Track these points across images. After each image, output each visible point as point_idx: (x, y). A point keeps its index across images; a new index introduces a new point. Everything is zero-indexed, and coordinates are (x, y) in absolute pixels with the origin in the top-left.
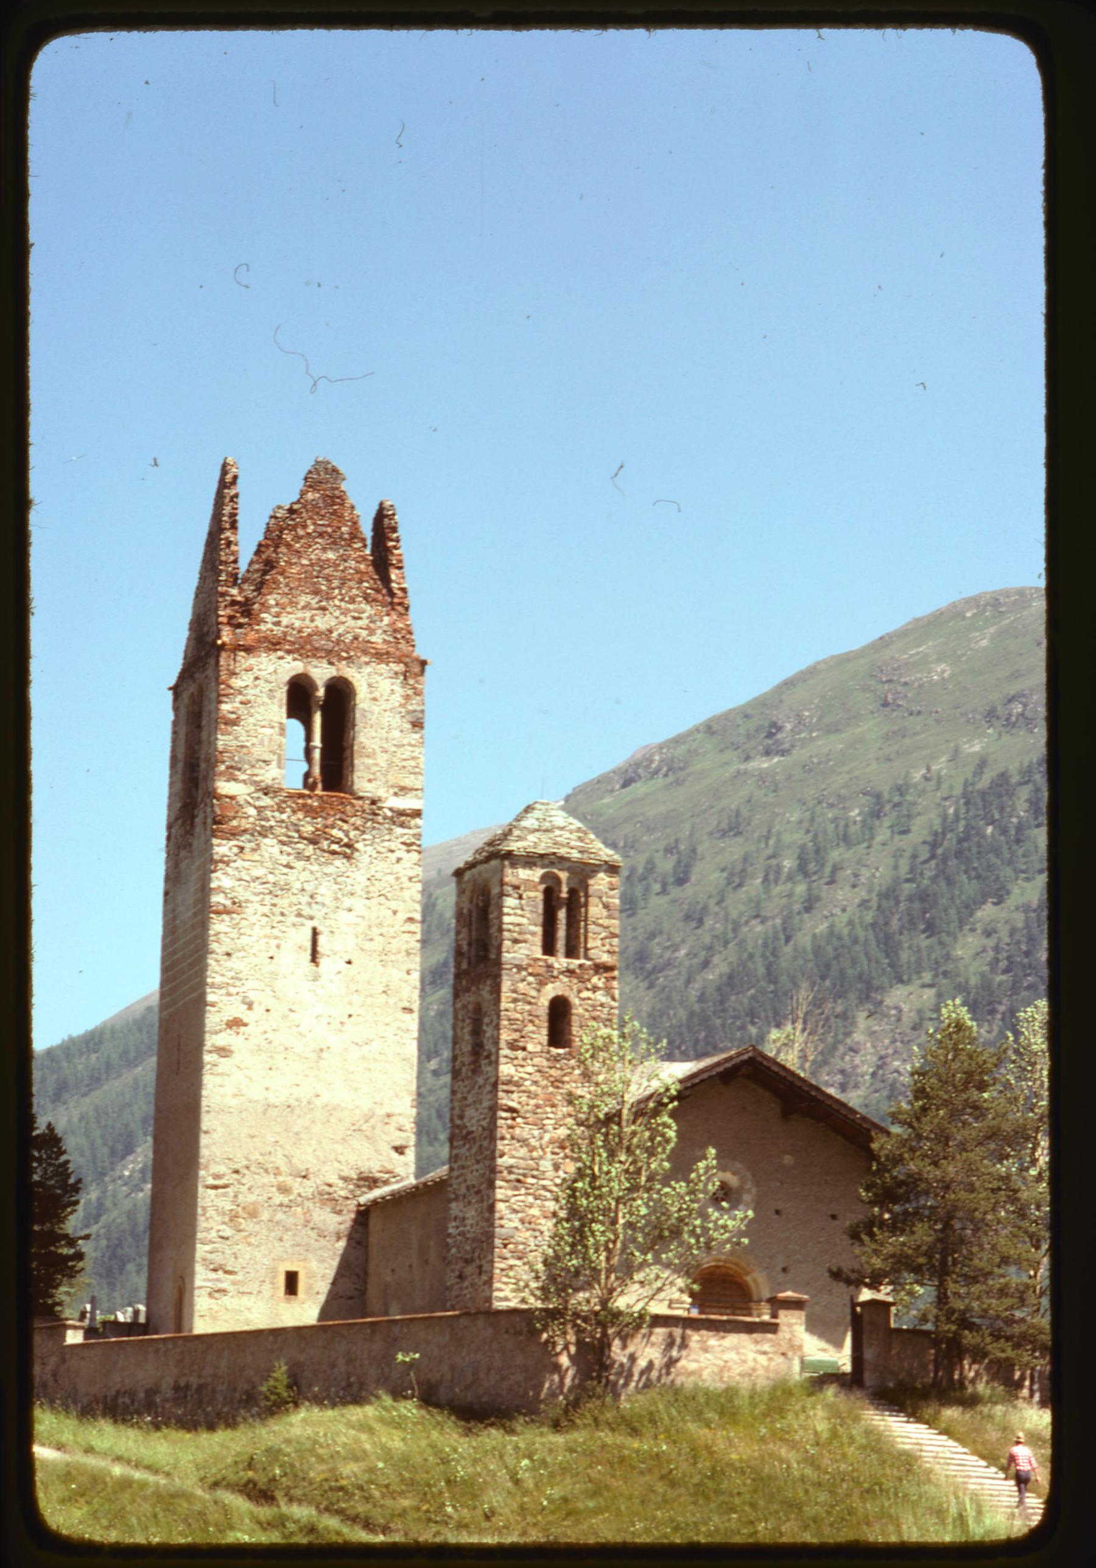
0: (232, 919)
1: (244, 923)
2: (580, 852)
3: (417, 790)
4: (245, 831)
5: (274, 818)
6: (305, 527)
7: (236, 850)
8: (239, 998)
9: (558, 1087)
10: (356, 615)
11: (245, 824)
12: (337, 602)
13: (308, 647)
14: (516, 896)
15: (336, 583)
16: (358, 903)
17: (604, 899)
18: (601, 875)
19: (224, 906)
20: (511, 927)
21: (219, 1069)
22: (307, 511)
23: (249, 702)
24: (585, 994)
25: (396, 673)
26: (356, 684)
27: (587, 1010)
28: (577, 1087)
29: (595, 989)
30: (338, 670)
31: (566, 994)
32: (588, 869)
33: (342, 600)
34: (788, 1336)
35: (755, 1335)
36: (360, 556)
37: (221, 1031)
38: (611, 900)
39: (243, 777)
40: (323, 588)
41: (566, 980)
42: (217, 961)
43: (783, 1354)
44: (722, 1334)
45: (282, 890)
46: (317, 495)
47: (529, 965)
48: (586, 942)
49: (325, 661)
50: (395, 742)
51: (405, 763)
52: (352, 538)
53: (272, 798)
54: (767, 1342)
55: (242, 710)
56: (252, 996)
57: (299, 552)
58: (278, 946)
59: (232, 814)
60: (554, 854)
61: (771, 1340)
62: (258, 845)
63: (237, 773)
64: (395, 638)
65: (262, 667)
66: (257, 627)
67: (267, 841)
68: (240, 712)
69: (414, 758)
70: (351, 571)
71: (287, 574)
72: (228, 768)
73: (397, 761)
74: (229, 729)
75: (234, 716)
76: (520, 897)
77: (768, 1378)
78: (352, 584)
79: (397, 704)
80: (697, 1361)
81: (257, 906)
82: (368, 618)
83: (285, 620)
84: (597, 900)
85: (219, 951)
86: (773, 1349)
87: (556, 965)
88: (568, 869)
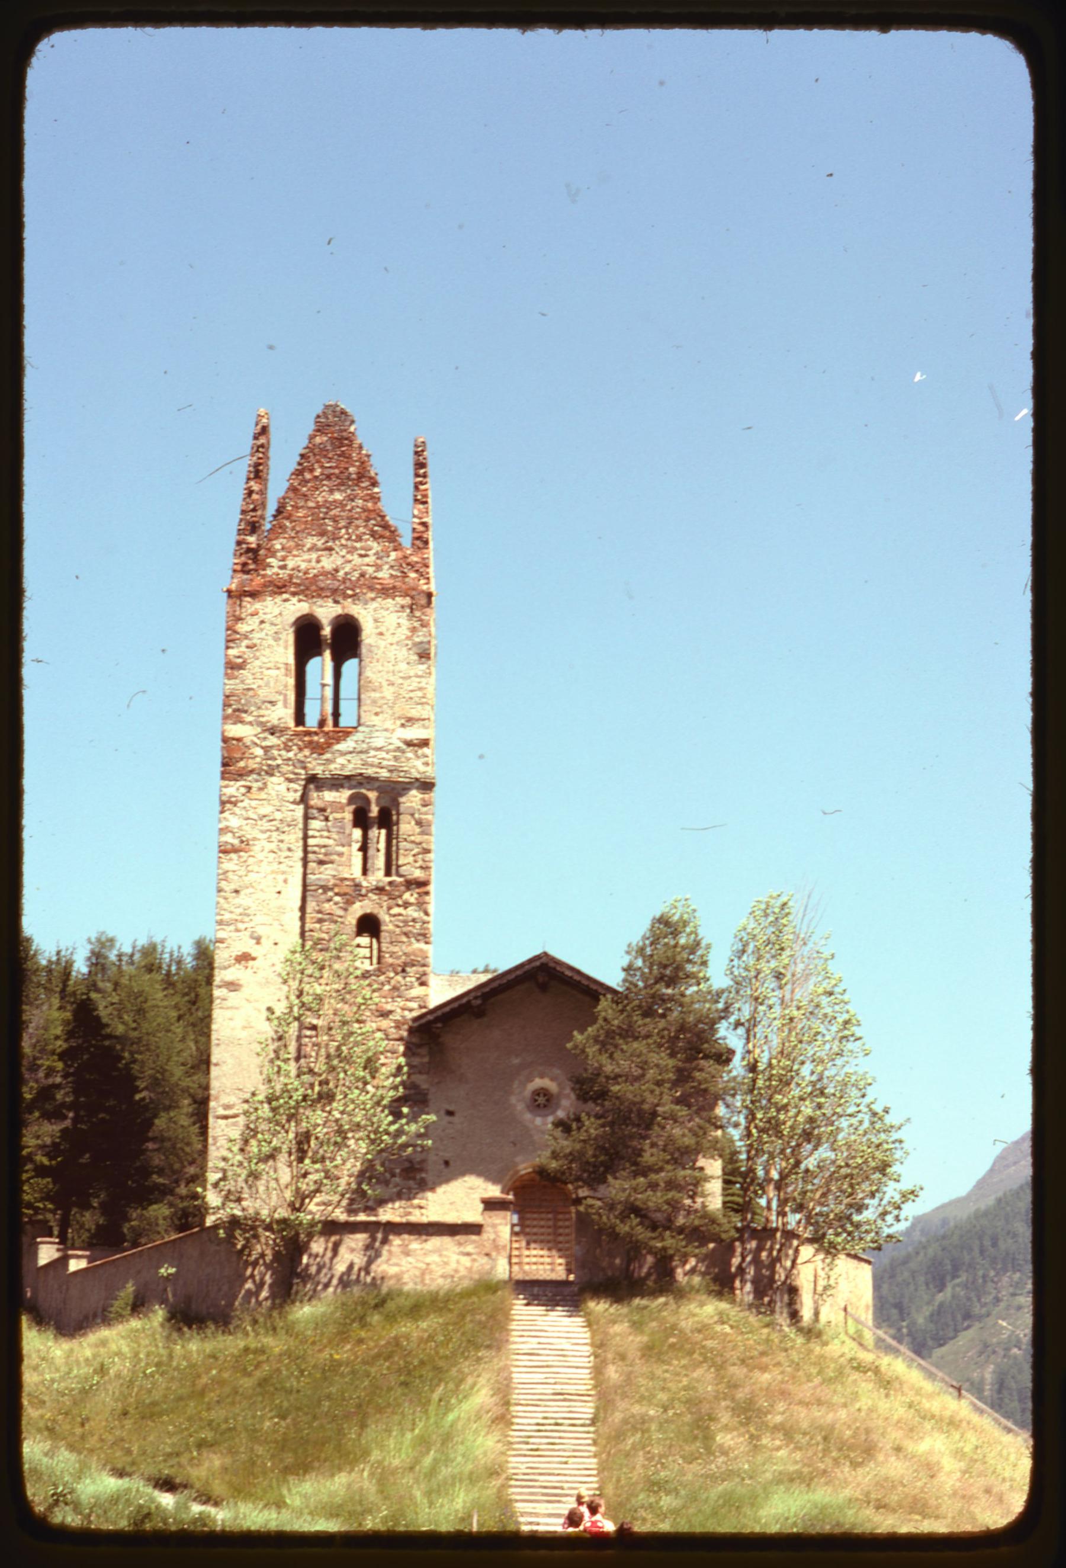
0: (240, 857)
1: (251, 860)
2: (390, 771)
3: (424, 720)
4: (252, 771)
5: (280, 756)
6: (312, 470)
7: (243, 790)
8: (248, 933)
10: (363, 552)
11: (252, 764)
12: (343, 542)
13: (314, 588)
14: (322, 818)
15: (342, 523)
17: (417, 816)
18: (414, 792)
19: (232, 845)
20: (316, 849)
21: (228, 1003)
22: (315, 455)
23: (255, 645)
25: (403, 607)
27: (398, 926)
28: (387, 1003)
29: (406, 905)
30: (343, 608)
31: (375, 911)
32: (398, 786)
33: (349, 539)
34: (492, 1236)
35: (458, 1237)
37: (230, 966)
38: (423, 817)
39: (249, 719)
40: (329, 528)
41: (375, 897)
43: (487, 1255)
44: (424, 1237)
45: (289, 826)
46: (325, 439)
47: (335, 885)
48: (397, 859)
49: (330, 600)
50: (401, 675)
51: (412, 695)
53: (279, 737)
54: (471, 1244)
55: (249, 654)
56: (260, 931)
57: (305, 496)
58: (285, 881)
60: (361, 774)
61: (474, 1242)
62: (265, 784)
63: (244, 715)
65: (267, 610)
67: (273, 779)
69: (420, 689)
70: (358, 510)
71: (294, 518)
74: (236, 673)
75: (240, 660)
76: (327, 819)
77: (471, 1279)
79: (404, 637)
80: (397, 1265)
81: (264, 843)
83: (291, 563)
84: (409, 817)
85: (227, 889)
86: (477, 1250)
87: (365, 884)
88: (378, 789)
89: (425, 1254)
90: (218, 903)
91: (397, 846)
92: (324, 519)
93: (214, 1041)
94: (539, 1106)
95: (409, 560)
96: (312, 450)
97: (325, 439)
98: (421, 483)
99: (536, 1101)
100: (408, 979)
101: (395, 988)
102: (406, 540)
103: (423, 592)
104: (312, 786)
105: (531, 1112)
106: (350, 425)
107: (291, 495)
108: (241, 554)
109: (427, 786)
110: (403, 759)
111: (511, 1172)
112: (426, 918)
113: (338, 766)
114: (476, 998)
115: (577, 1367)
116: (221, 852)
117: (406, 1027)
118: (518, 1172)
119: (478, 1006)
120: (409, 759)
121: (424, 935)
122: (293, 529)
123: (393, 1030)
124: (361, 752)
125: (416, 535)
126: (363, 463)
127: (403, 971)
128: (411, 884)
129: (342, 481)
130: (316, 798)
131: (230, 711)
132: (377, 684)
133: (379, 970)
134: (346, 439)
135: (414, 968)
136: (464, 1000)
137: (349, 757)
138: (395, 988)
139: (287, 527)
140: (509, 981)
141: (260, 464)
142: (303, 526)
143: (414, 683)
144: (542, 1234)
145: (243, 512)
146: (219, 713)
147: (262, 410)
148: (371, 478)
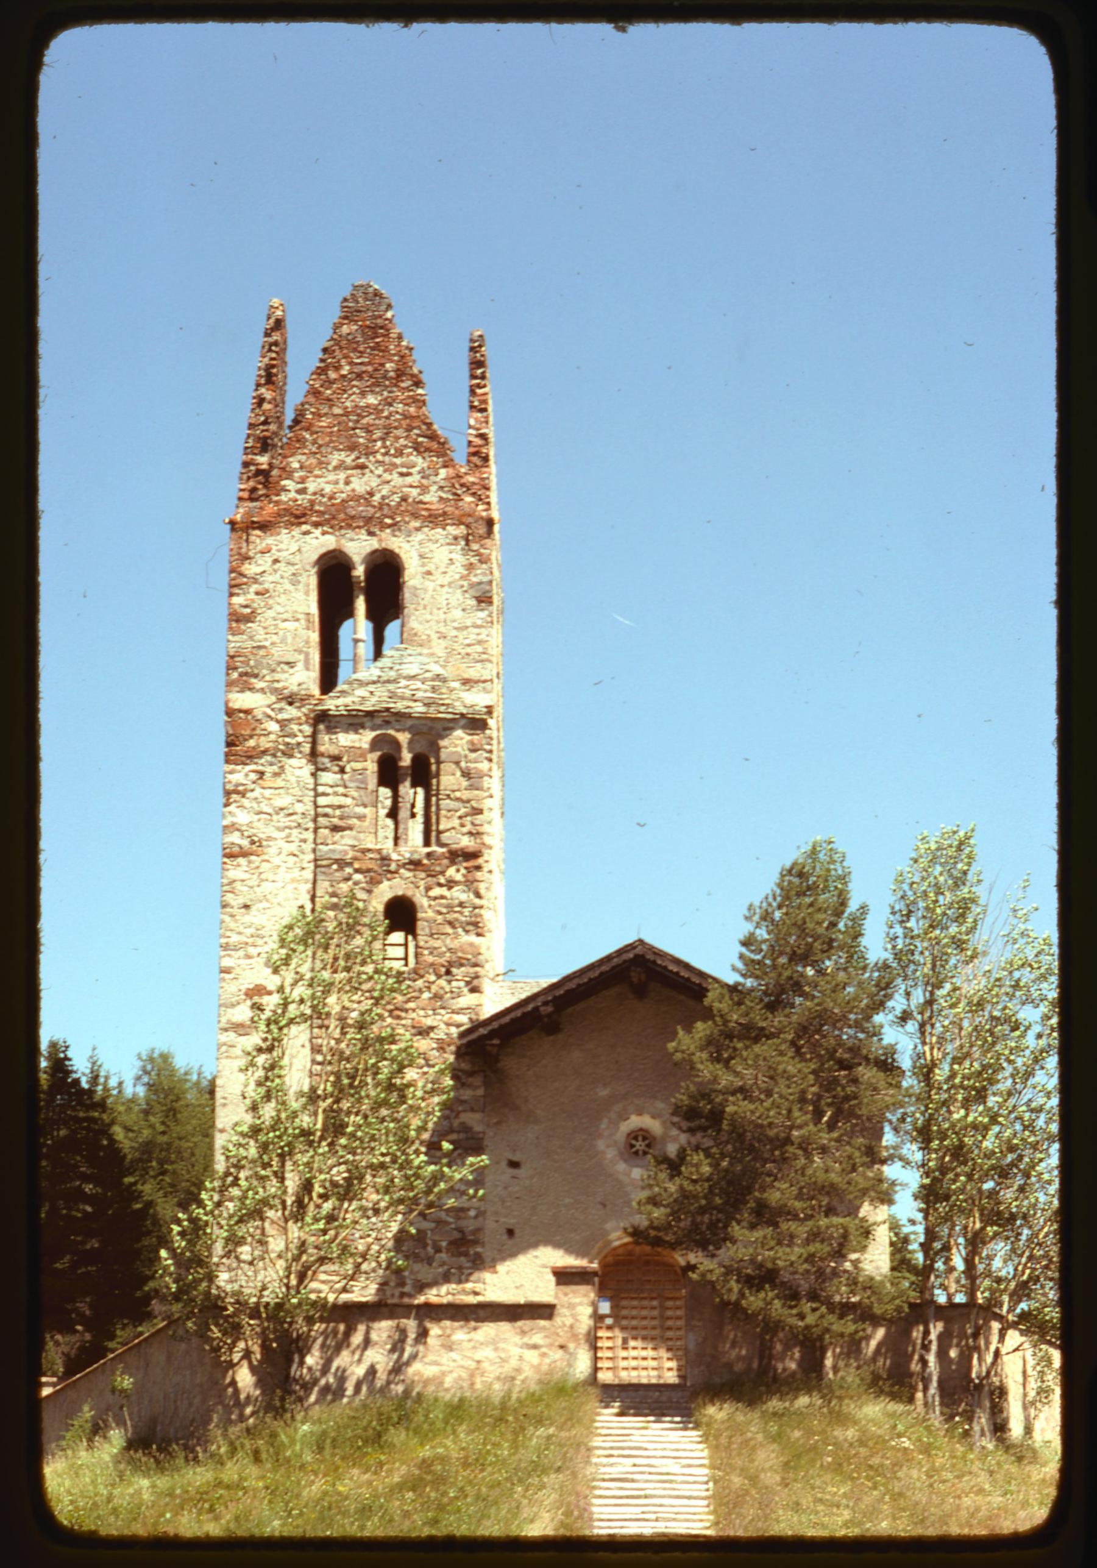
0: (250, 862)
1: (265, 866)
2: (425, 705)
3: (485, 681)
4: (264, 752)
6: (337, 368)
7: (253, 776)
8: (262, 960)
9: (399, 1018)
10: (404, 470)
11: (264, 743)
12: (379, 457)
14: (336, 769)
15: (378, 434)
17: (463, 764)
18: (459, 733)
19: (240, 847)
20: (329, 810)
22: (341, 348)
23: (267, 591)
24: (436, 891)
25: (456, 538)
26: (404, 556)
27: (440, 913)
29: (451, 884)
30: (380, 540)
31: (409, 893)
33: (386, 454)
34: (569, 1321)
35: (520, 1323)
36: (409, 397)
40: (361, 440)
42: (232, 916)
43: (562, 1347)
44: (473, 1324)
46: (355, 327)
47: (356, 859)
48: (438, 823)
49: (363, 531)
50: (456, 625)
51: (469, 650)
52: (398, 376)
53: (299, 708)
54: (538, 1331)
55: (259, 602)
57: (329, 400)
59: (248, 732)
60: (388, 709)
61: (544, 1328)
62: (282, 768)
63: (253, 680)
64: (455, 494)
65: (281, 546)
66: (275, 498)
67: (293, 762)
68: (255, 605)
69: (480, 642)
70: (398, 416)
72: (241, 675)
73: (459, 649)
75: (248, 611)
76: (342, 771)
78: (400, 432)
79: (457, 576)
81: (281, 843)
82: (419, 472)
84: (453, 766)
85: (233, 903)
86: (548, 1341)
87: (394, 856)
88: (409, 729)
89: (474, 1347)
90: (222, 922)
91: (438, 805)
92: (354, 429)
93: (219, 1101)
94: (636, 1153)
95: (463, 481)
96: (337, 343)
97: (355, 327)
98: (479, 386)
99: (632, 1146)
100: (454, 984)
101: (437, 997)
102: (460, 455)
103: (482, 518)
104: (321, 727)
105: (626, 1161)
106: (387, 310)
107: (312, 399)
108: (249, 478)
109: (476, 724)
110: (444, 690)
111: (600, 1244)
112: (477, 901)
113: (356, 700)
114: (545, 1003)
115: (689, 1498)
116: (225, 856)
117: (453, 1048)
118: (610, 1242)
119: (549, 1015)
120: (452, 690)
121: (476, 924)
122: (314, 442)
123: (435, 1053)
124: (388, 681)
125: (472, 450)
126: (402, 357)
127: (448, 972)
128: (457, 856)
129: (377, 380)
130: (327, 743)
131: (235, 675)
132: (424, 637)
133: (415, 971)
134: (382, 328)
135: (463, 969)
136: (530, 1007)
137: (371, 688)
138: (437, 997)
139: (306, 440)
140: (590, 980)
141: (273, 366)
142: (328, 439)
143: (472, 635)
144: (645, 1328)
145: (251, 426)
146: (222, 679)
147: (275, 300)
148: (413, 376)
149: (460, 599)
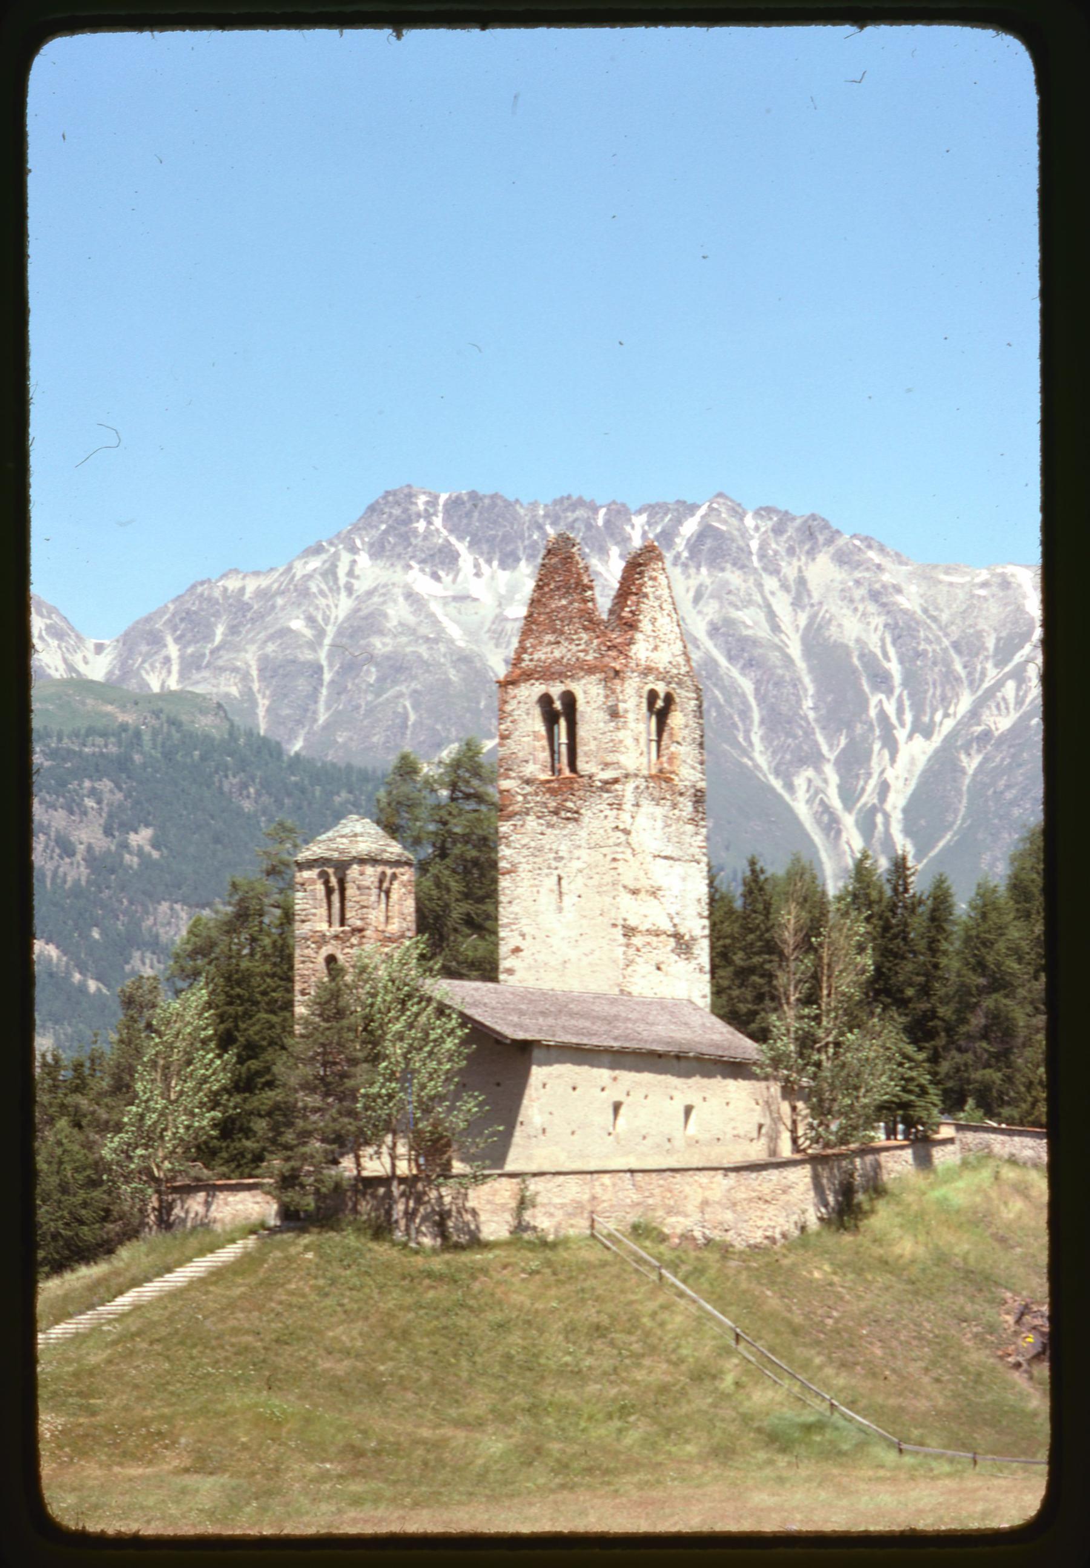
4: (516, 814)
16: (583, 853)
18: (355, 866)
29: (352, 946)
56: (525, 930)
67: (529, 818)
83: (536, 657)
149: (604, 716)
